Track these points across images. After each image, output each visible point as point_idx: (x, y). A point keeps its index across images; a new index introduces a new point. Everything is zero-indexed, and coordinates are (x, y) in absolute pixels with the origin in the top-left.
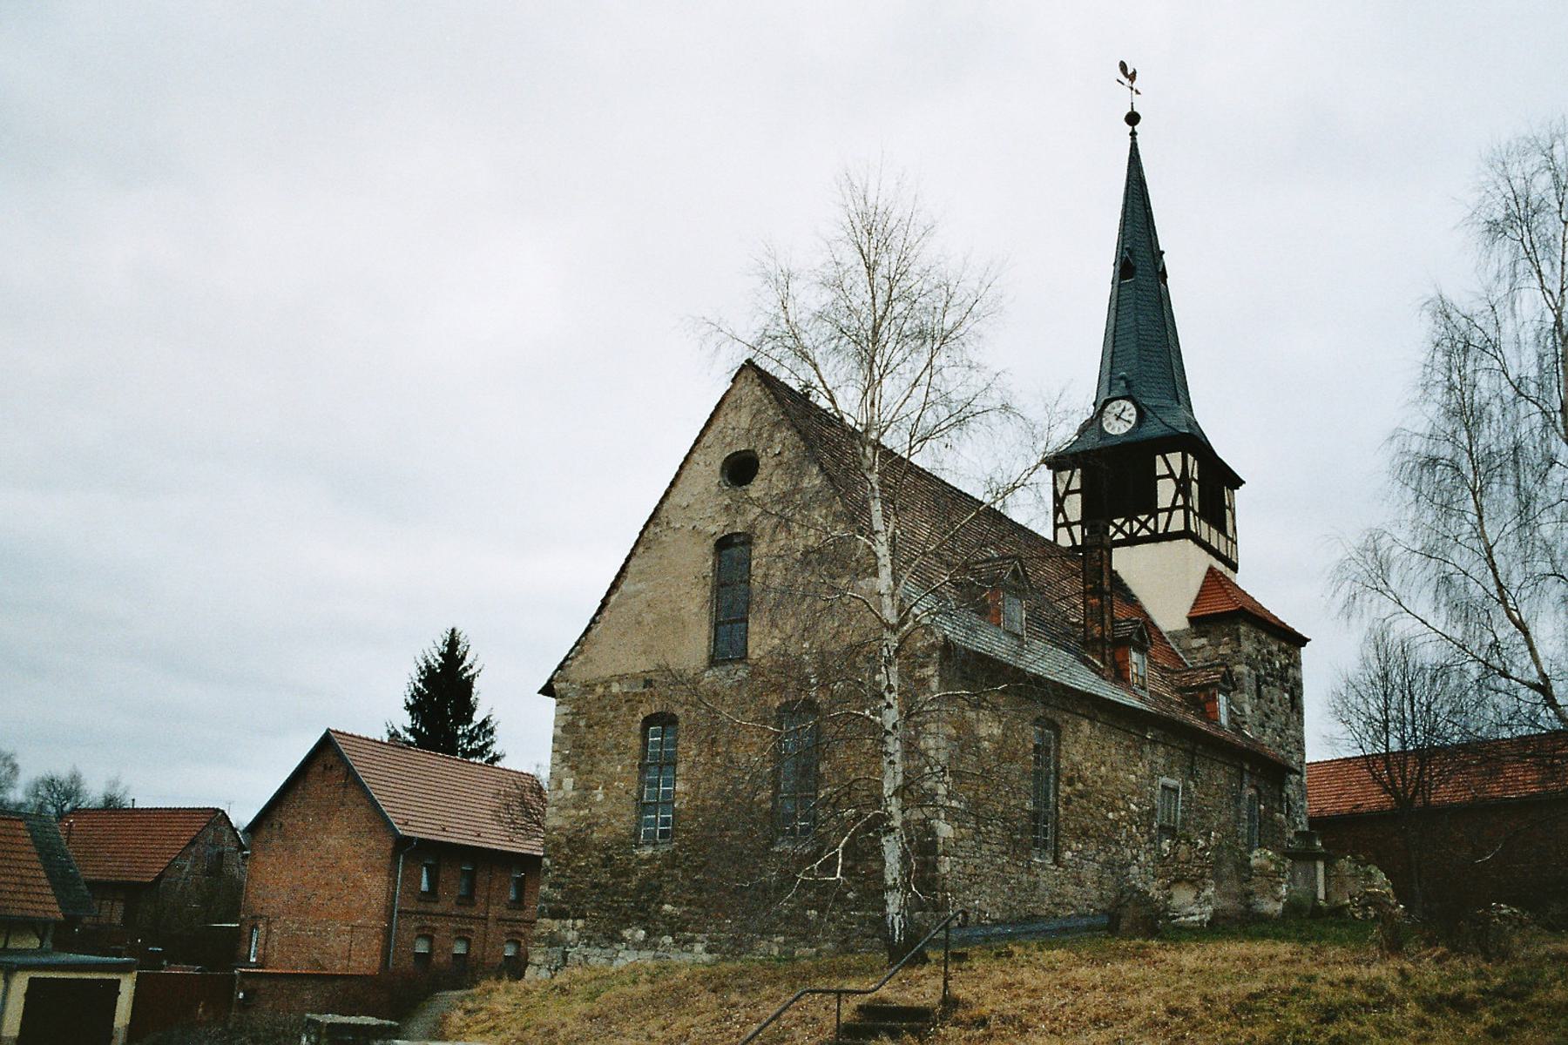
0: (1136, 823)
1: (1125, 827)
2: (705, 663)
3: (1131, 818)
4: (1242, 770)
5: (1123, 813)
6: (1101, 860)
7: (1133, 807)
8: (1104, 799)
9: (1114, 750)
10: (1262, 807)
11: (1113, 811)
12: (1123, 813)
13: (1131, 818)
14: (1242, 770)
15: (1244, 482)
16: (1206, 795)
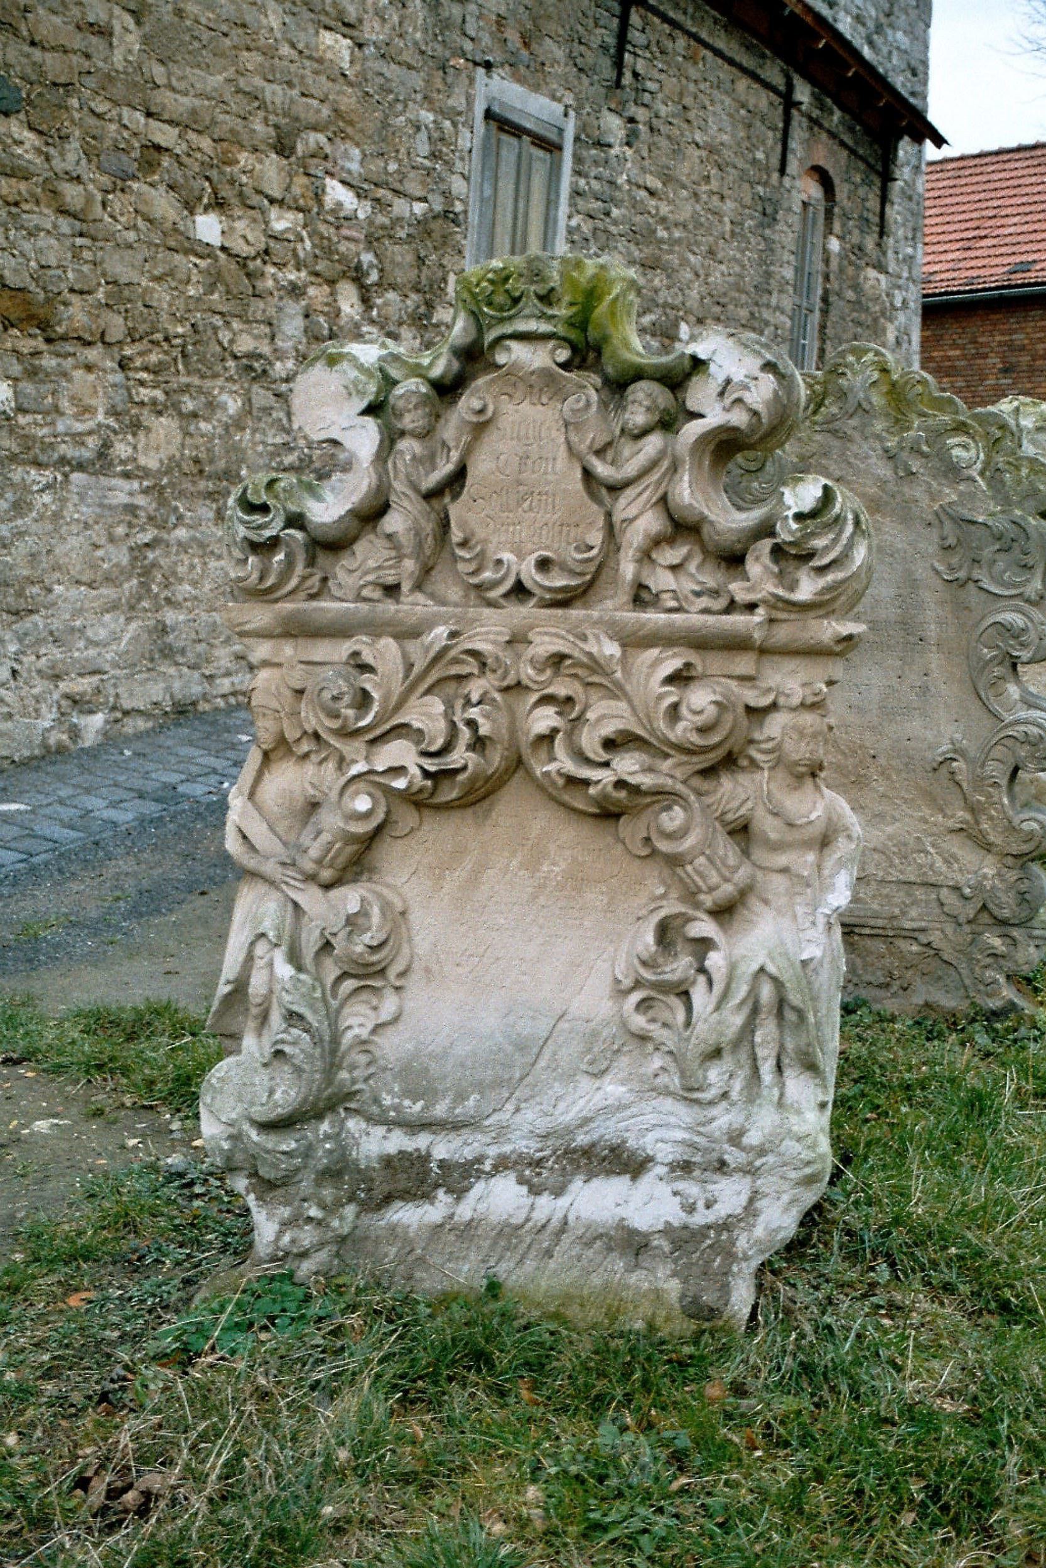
0: (357, 275)
1: (296, 291)
2: (93, 1483)
3: (326, 249)
4: (789, 103)
5: (282, 222)
6: (151, 462)
7: (337, 193)
8: (165, 135)
9: (663, 786)
10: (834, 245)
11: (219, 204)
12: (282, 222)
13: (326, 249)
14: (789, 103)
15: (946, 142)
16: (667, 178)
